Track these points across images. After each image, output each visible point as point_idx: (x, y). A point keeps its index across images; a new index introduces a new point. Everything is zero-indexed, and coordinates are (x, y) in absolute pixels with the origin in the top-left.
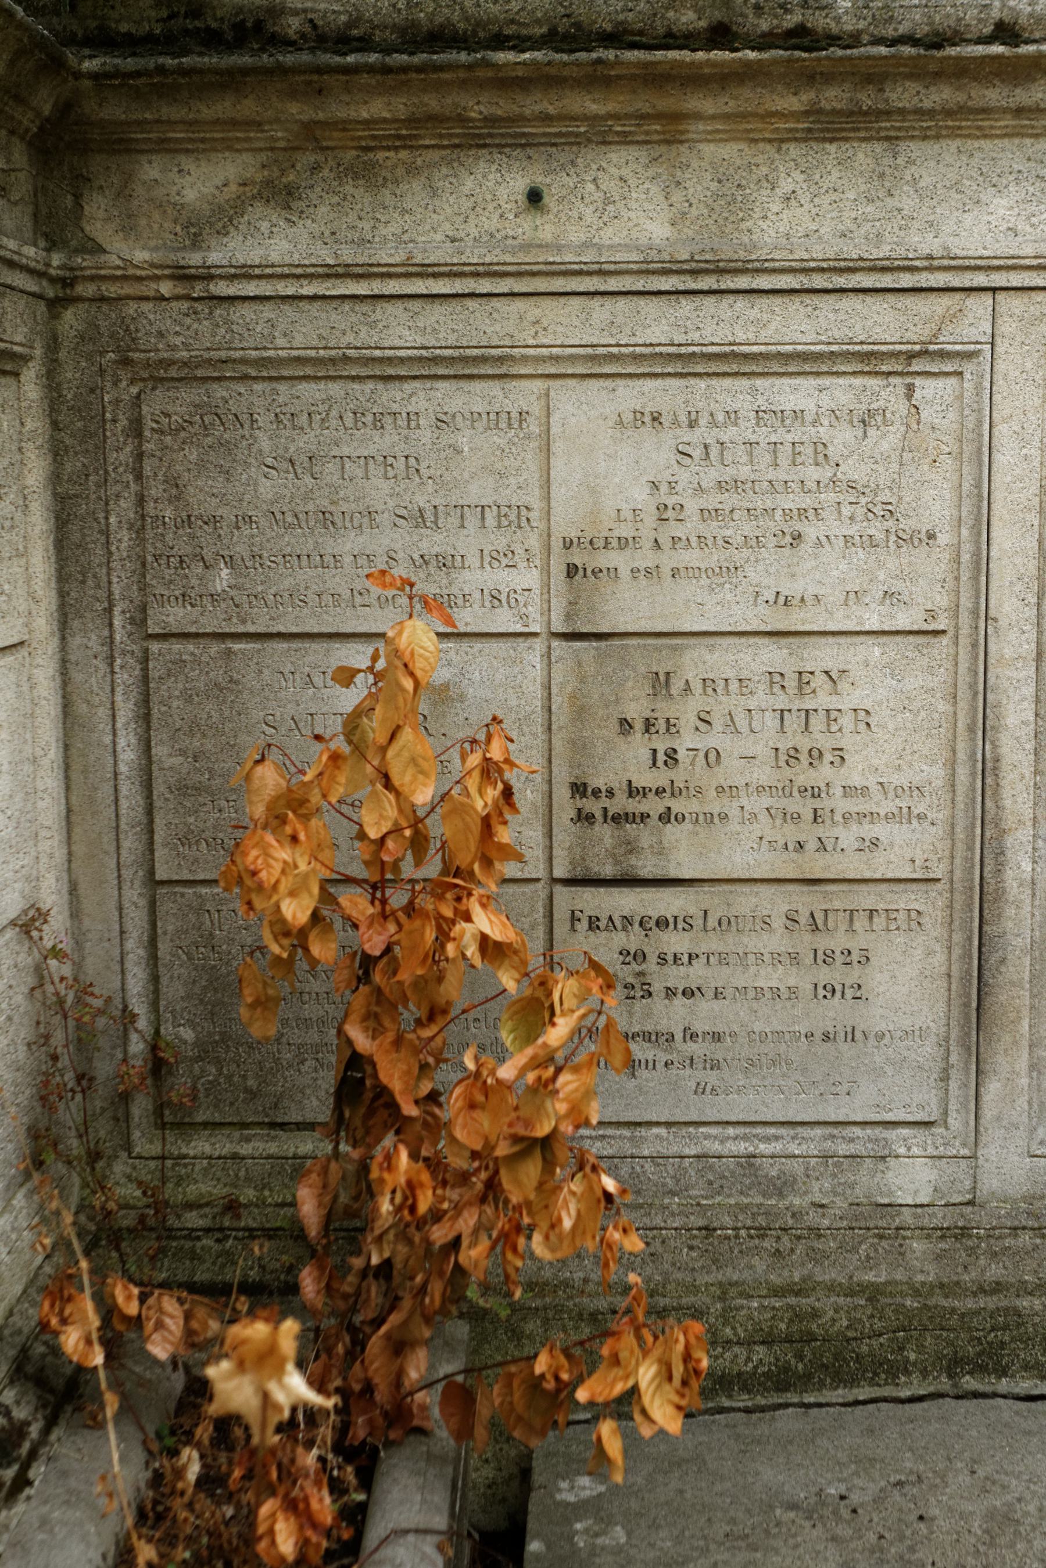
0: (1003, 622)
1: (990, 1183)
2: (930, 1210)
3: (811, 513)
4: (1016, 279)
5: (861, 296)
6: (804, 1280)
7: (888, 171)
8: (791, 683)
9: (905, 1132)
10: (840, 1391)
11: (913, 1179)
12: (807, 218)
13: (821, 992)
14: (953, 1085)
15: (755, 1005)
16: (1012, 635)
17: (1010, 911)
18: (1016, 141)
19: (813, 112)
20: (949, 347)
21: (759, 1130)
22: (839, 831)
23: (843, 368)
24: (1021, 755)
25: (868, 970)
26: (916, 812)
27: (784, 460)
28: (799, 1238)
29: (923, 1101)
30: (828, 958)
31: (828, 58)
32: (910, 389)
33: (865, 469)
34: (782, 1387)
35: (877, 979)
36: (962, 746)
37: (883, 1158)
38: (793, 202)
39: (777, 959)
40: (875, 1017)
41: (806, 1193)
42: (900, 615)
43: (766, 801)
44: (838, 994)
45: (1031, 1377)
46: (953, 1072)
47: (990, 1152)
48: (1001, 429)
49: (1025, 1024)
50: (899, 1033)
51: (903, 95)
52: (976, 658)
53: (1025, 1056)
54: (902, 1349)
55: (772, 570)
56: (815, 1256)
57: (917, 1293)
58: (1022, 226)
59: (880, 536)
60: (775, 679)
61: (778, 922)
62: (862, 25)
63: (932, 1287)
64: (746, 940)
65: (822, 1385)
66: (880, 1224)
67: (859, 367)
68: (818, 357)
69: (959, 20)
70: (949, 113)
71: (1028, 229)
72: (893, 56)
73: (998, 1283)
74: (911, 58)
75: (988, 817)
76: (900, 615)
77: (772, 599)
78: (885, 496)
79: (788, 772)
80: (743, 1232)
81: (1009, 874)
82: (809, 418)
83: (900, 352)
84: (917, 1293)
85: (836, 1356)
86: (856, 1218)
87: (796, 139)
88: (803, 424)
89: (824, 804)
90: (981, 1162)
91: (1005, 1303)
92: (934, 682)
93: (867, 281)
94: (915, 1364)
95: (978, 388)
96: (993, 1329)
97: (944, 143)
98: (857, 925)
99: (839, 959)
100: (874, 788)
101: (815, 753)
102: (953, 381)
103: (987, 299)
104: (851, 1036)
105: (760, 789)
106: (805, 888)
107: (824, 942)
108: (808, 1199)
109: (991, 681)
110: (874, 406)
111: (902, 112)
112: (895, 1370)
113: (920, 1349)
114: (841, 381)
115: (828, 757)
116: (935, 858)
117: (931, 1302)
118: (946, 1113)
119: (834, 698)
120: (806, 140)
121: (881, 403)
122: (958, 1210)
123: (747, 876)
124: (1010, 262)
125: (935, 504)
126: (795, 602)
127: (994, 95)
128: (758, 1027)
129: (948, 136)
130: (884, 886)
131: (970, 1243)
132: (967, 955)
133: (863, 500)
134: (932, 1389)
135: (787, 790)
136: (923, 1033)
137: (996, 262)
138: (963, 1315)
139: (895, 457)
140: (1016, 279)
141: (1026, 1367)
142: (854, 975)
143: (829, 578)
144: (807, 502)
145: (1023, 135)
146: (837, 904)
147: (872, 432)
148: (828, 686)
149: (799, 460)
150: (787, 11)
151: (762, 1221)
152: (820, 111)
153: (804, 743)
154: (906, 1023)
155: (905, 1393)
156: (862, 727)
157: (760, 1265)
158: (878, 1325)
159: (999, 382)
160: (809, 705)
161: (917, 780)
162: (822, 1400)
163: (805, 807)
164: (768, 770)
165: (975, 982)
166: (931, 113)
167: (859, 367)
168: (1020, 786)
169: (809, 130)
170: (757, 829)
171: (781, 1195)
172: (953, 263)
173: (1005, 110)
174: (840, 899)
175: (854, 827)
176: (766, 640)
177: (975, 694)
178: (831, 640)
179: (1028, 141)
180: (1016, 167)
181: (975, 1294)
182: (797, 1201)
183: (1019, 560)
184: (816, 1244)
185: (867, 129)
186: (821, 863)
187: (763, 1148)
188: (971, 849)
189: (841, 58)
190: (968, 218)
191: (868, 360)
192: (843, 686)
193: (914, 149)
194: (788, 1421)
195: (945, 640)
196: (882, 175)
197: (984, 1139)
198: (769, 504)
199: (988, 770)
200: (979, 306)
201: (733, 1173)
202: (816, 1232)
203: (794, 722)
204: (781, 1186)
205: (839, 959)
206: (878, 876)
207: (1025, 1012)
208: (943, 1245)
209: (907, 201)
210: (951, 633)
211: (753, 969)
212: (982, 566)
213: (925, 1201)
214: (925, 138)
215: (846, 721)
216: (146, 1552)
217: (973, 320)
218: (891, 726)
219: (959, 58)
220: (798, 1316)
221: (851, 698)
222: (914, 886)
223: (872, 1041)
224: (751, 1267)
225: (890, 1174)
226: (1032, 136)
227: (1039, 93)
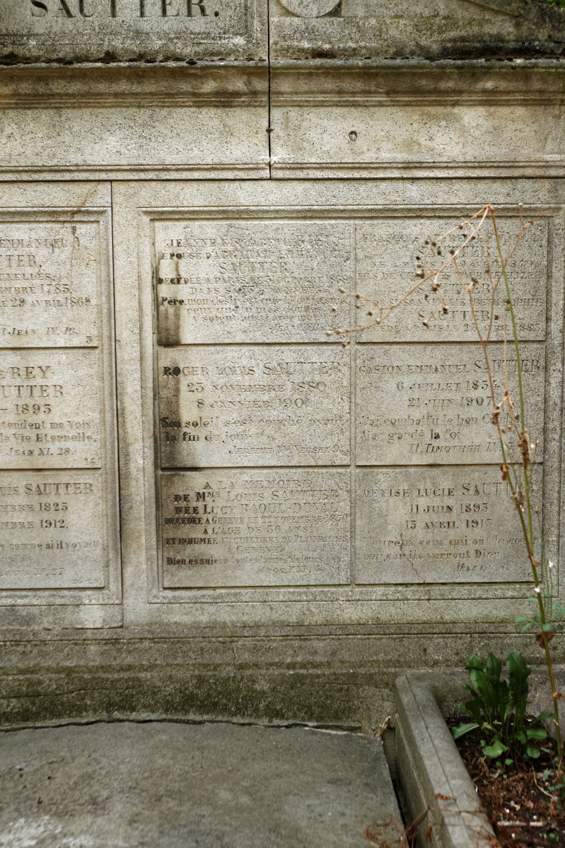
0: (123, 342)
1: (130, 617)
2: (101, 631)
3: (29, 289)
4: (120, 176)
5: (47, 184)
6: (35, 666)
7: (57, 123)
8: (23, 373)
9: (89, 592)
10: (54, 721)
11: (93, 616)
12: (19, 146)
13: (45, 524)
14: (111, 569)
15: (12, 531)
16: (128, 349)
17: (133, 483)
18: (118, 109)
19: (15, 94)
20: (91, 209)
21: (18, 593)
22: (49, 445)
23: (41, 219)
24: (135, 407)
25: (67, 513)
26: (87, 435)
27: (14, 264)
28: (36, 645)
29: (95, 577)
30: (47, 508)
31: (16, 68)
32: (74, 229)
33: (54, 268)
34: (26, 719)
35: (72, 518)
36: (107, 403)
37: (78, 605)
38: (12, 138)
39: (22, 508)
40: (71, 536)
41: (41, 623)
42: (74, 339)
43: (13, 431)
44: (53, 525)
45: (147, 712)
46: (111, 562)
47: (129, 601)
48: (118, 249)
50: (84, 544)
51: (58, 87)
52: (111, 360)
53: (144, 554)
54: (83, 699)
55: (11, 317)
56: (42, 654)
57: (90, 671)
58: (123, 150)
59: (63, 301)
60: (15, 371)
61: (22, 490)
62: (41, 53)
63: (97, 668)
64: (6, 499)
65: (45, 718)
66: (76, 637)
67: (49, 219)
68: (28, 214)
69: (88, 51)
70: (83, 96)
71: (126, 152)
72: (48, 68)
73: (130, 666)
74: (57, 68)
75: (120, 437)
76: (74, 339)
77: (11, 331)
79: (23, 416)
80: (8, 643)
81: (132, 465)
82: (25, 243)
83: (67, 212)
84: (90, 671)
85: (52, 703)
86: (64, 635)
87: (12, 108)
88: (23, 246)
89: (42, 432)
90: (125, 606)
91: (133, 675)
92: (93, 371)
93: (49, 176)
94: (90, 706)
95: (106, 228)
96: (127, 688)
97: (84, 110)
98: (60, 491)
99: (53, 508)
100: (66, 424)
101: (36, 407)
102: (95, 225)
103: (108, 185)
105: (10, 425)
106: (35, 473)
107: (44, 500)
108: (42, 626)
109: (118, 371)
110: (57, 237)
111: (59, 94)
112: (81, 709)
113: (92, 698)
114: (41, 225)
115: (43, 409)
116: (97, 458)
117: (97, 675)
118: (108, 584)
119: (44, 380)
120: (17, 108)
121: (61, 236)
122: (114, 630)
123: (5, 467)
124: (116, 168)
125: (89, 284)
126: (23, 333)
127: (102, 87)
128: (14, 542)
129: (84, 107)
130: (74, 472)
131: (119, 646)
132: (114, 505)
133: (54, 283)
134: (98, 718)
135: (23, 425)
136: (96, 544)
137: (109, 168)
138: (112, 682)
139: (68, 262)
140: (120, 176)
141: (144, 707)
142: (60, 515)
143: (39, 321)
144: (27, 284)
145: (121, 107)
146: (50, 481)
147: (56, 250)
148: (41, 374)
149: (22, 264)
150: (4, 46)
151: (18, 637)
152: (19, 94)
153: (31, 402)
154: (87, 539)
155: (85, 720)
156: (59, 393)
157: (14, 658)
158: (71, 687)
159: (116, 225)
160: (32, 383)
161: (86, 419)
162: (44, 725)
163: (32, 434)
164: (13, 415)
165: (118, 518)
166: (73, 95)
167: (49, 219)
168: (135, 422)
169: (17, 104)
170: (9, 444)
171: (29, 625)
172: (89, 168)
173: (109, 94)
174: (52, 478)
175: (57, 443)
176: (10, 352)
177: (112, 378)
178: (42, 351)
179: (124, 109)
180: (119, 122)
181: (118, 671)
182: (36, 628)
183: (129, 312)
184: (44, 648)
185: (45, 103)
186: (42, 461)
187: (19, 601)
188: (113, 453)
189: (23, 69)
190: (97, 147)
191: (53, 215)
192: (48, 374)
193: (69, 113)
194: (22, 735)
195: (97, 351)
196: (54, 126)
197: (126, 595)
198: (8, 285)
199: (119, 414)
200: (104, 189)
201: (4, 614)
202: (44, 642)
203: (25, 392)
204: (29, 620)
205: (53, 508)
206: (69, 467)
207: (143, 533)
208: (106, 648)
209: (67, 138)
210: (100, 348)
211: (10, 513)
212: (112, 315)
213: (99, 626)
214: (74, 108)
215: (51, 391)
217: (101, 196)
218: (73, 394)
219: (79, 69)
220: (31, 684)
221: (53, 380)
222: (88, 472)
223: (71, 548)
224: (10, 660)
225: (81, 613)
226: (125, 107)
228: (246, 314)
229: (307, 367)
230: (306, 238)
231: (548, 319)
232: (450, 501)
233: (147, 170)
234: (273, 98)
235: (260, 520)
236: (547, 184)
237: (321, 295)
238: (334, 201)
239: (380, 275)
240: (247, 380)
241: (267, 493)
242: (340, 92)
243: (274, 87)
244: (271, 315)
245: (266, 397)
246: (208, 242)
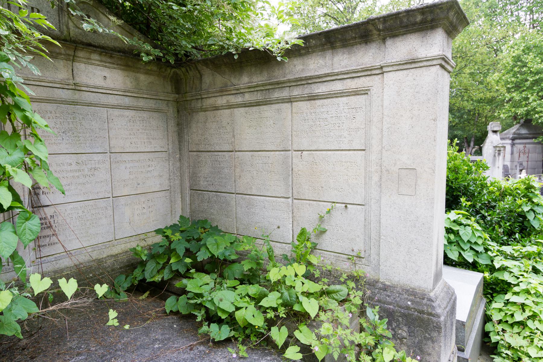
216: (540, 344)
228: (67, 142)
229: (93, 162)
230: (89, 114)
231: (168, 145)
232: (144, 206)
233: (30, 80)
234: (75, 58)
235: (78, 223)
236: (166, 102)
237: (96, 135)
238: (99, 101)
239: (117, 129)
240: (69, 168)
241: (80, 212)
242: (101, 61)
243: (76, 54)
244: (77, 142)
245: (77, 174)
246: (49, 112)
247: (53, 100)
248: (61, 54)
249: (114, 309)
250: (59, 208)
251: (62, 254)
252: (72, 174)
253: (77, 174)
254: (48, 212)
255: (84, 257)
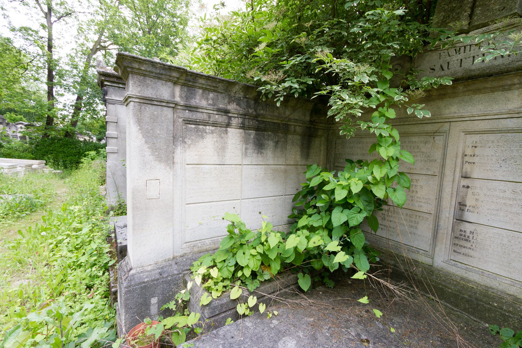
32: (434, 138)
49: (445, 241)
68: (419, 133)
78: (428, 154)
104: (414, 234)
142: (416, 225)
174: (415, 213)
192: (418, 182)
215: (418, 187)
216: (2, 201)
227: (521, 115)
245: (511, 202)
247: (497, 131)
248: (514, 84)
249: (368, 299)
250: (479, 229)
251: (474, 268)
252: (504, 201)
253: (511, 202)
254: (468, 228)
255: (498, 285)
